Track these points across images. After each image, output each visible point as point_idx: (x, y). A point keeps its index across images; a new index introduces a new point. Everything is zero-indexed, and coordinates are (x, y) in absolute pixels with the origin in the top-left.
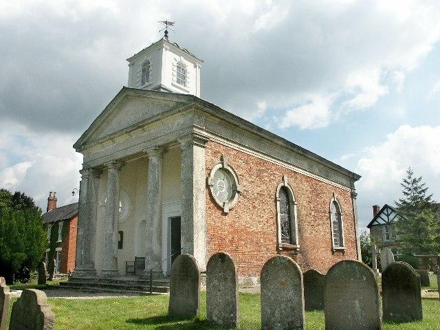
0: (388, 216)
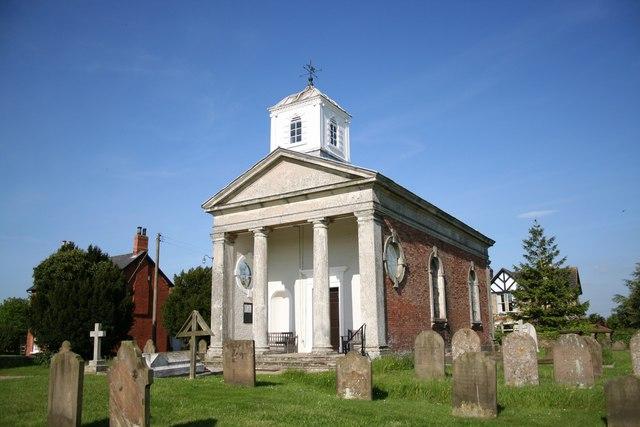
0: (505, 282)
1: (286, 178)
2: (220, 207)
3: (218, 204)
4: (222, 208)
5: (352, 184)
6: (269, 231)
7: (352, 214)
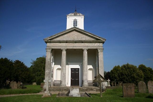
1: (75, 36)
2: (51, 41)
3: (50, 40)
4: (51, 41)
5: (97, 41)
6: (67, 50)
7: (97, 49)
